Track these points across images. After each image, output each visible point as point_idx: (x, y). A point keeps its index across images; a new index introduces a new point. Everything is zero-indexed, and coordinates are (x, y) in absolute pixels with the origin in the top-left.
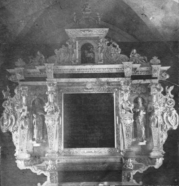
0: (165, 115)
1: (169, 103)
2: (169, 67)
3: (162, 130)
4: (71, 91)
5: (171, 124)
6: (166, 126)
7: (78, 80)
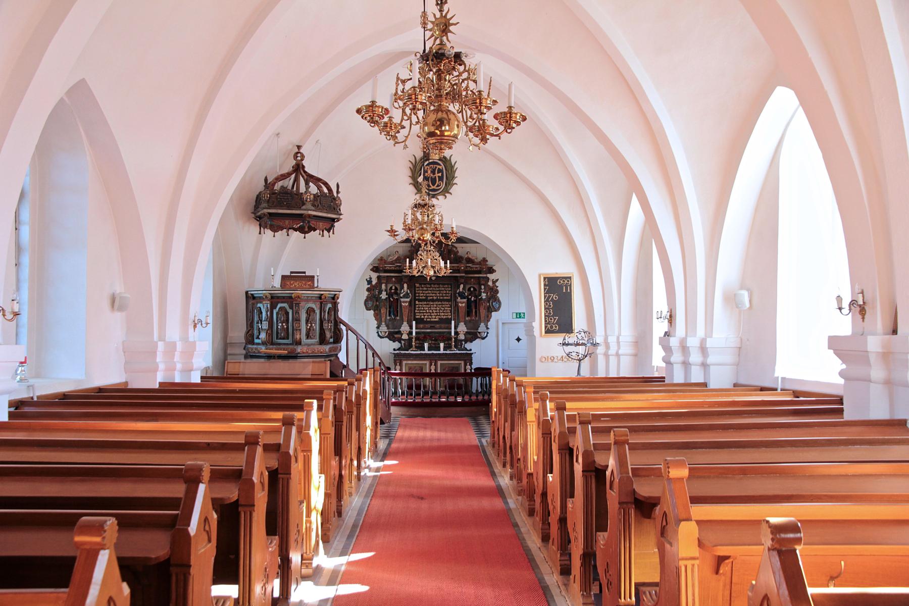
0: (491, 302)
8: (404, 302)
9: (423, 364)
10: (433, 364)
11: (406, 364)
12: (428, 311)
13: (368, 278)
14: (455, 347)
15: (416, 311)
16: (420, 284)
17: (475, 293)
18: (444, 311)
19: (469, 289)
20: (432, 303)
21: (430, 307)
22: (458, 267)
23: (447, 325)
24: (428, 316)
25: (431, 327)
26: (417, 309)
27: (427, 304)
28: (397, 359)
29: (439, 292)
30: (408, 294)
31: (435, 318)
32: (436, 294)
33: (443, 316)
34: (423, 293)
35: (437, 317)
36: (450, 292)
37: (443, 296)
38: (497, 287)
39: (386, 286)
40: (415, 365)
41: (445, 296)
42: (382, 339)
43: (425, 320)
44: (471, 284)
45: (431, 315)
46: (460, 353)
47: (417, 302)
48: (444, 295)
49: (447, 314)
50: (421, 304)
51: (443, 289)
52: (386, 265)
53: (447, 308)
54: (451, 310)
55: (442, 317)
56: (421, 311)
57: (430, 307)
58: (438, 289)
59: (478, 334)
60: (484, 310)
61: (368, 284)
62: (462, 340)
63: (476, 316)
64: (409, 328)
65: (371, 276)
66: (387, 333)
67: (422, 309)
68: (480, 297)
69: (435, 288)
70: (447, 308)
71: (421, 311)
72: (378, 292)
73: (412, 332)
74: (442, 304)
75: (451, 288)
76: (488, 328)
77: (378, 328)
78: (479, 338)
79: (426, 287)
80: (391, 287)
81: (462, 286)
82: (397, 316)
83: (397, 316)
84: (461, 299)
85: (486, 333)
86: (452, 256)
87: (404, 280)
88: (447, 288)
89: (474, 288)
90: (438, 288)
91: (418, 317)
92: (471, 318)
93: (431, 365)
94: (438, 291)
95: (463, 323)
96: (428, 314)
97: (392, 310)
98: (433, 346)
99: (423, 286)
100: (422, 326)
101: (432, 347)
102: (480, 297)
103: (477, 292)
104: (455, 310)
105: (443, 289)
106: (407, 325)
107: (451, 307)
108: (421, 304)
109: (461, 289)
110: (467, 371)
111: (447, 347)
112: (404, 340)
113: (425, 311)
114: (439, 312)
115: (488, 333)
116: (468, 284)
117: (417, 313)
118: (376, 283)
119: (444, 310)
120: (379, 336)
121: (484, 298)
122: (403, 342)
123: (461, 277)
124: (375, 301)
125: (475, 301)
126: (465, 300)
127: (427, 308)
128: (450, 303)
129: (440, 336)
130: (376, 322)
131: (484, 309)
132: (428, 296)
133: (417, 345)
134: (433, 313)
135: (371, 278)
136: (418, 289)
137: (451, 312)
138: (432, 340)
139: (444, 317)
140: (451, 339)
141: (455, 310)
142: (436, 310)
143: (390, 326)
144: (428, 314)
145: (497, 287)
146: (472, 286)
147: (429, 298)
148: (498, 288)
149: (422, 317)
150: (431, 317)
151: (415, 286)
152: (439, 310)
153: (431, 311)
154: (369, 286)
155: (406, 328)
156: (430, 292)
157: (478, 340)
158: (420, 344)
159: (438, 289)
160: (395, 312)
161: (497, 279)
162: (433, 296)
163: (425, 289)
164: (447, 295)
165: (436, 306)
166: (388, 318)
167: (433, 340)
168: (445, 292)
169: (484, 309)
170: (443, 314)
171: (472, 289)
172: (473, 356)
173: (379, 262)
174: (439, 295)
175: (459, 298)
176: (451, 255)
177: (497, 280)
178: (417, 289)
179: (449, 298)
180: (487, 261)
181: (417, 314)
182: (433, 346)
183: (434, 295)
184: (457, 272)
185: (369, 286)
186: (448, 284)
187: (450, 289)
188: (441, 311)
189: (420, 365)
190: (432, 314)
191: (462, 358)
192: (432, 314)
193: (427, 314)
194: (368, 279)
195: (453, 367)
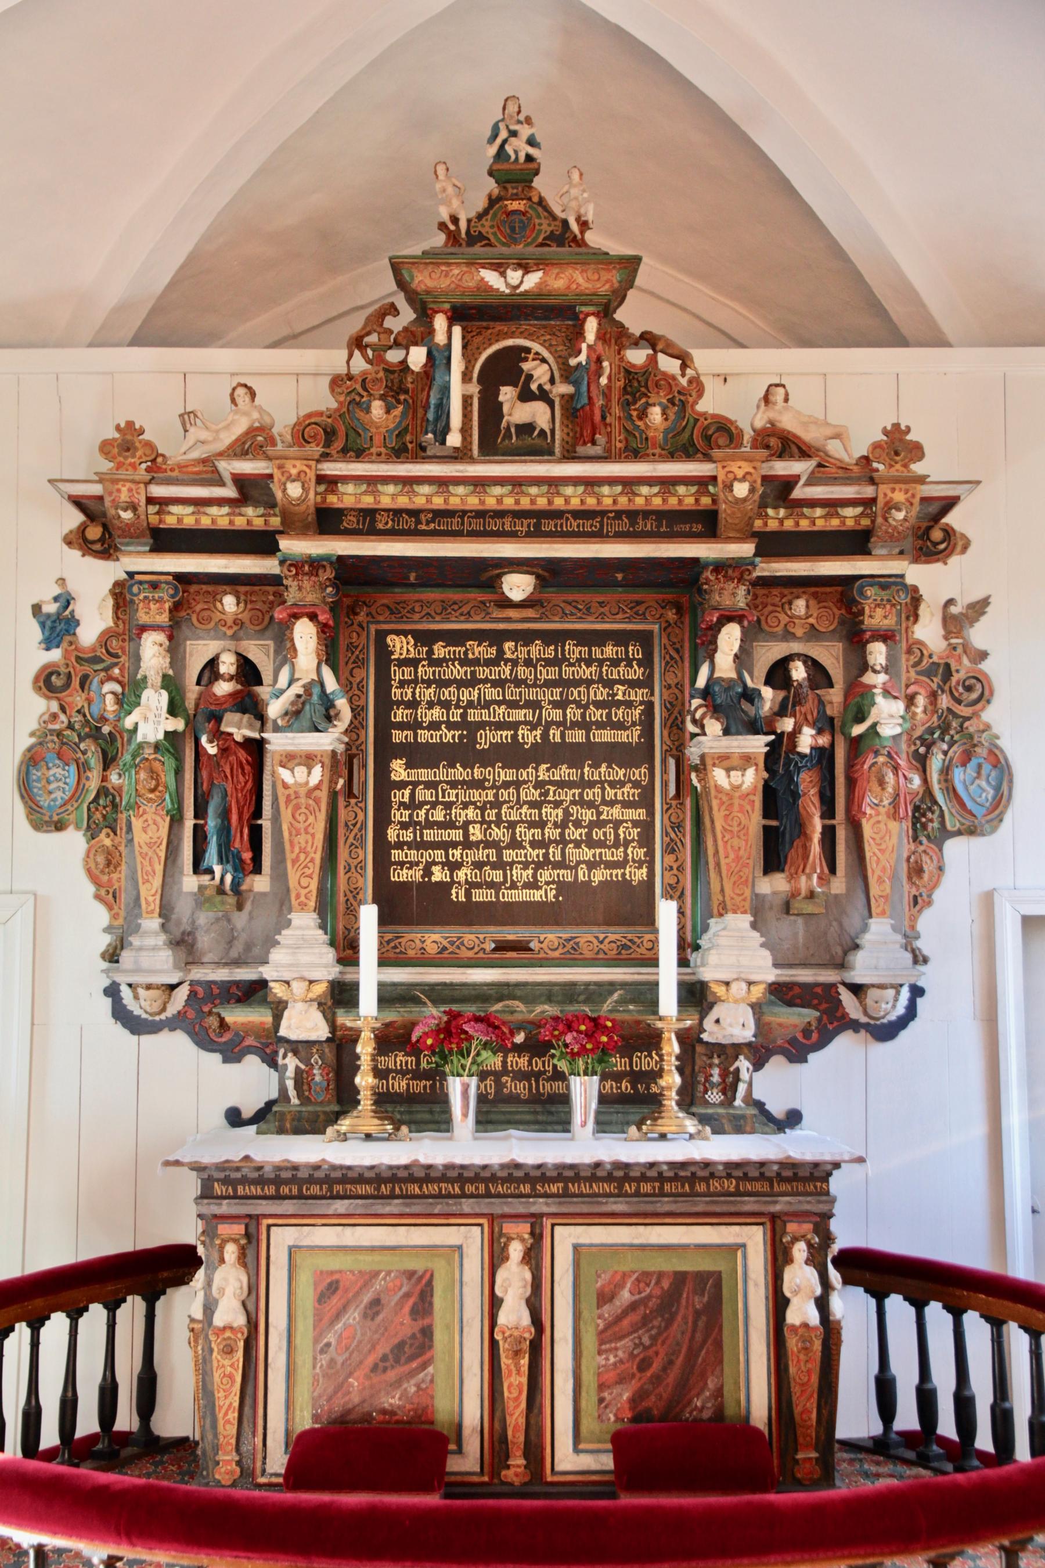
0: (936, 763)
1: (961, 689)
2: (941, 1451)
3: (915, 838)
4: (381, 618)
5: (969, 805)
6: (942, 815)
7: (597, 551)
8: (289, 759)
9: (431, 1249)
10: (516, 1250)
11: (292, 1251)
12: (476, 833)
13: (46, 594)
14: (688, 1099)
15: (392, 834)
16: (425, 638)
17: (821, 703)
18: (598, 834)
19: (778, 676)
20: (506, 775)
21: (497, 804)
22: (703, 483)
23: (615, 935)
24: (478, 865)
25: (502, 947)
26: (399, 815)
27: (479, 784)
28: (225, 1208)
29: (556, 693)
30: (328, 703)
31: (533, 885)
32: (534, 705)
33: (592, 865)
34: (446, 705)
35: (545, 875)
36: (639, 695)
37: (585, 725)
38: (983, 655)
39: (175, 650)
40: (366, 1263)
41: (601, 725)
42: (147, 1040)
43: (458, 895)
44: (788, 636)
45: (500, 865)
46: (735, 1169)
47: (399, 770)
48: (598, 715)
49: (619, 854)
50: (431, 785)
51: (587, 672)
52: (158, 491)
53: (616, 812)
54: (646, 828)
55: (582, 874)
56: (429, 835)
57: (497, 804)
58: (552, 673)
59: (846, 997)
60: (894, 826)
61: (49, 643)
62: (737, 1049)
63: (833, 870)
64: (330, 955)
65: (72, 587)
66: (182, 994)
67: (439, 815)
68: (857, 730)
69: (528, 663)
70: (616, 812)
71: (429, 835)
72: (119, 700)
73: (354, 987)
74: (584, 784)
75: (647, 662)
76: (919, 959)
77: (112, 956)
78: (855, 1026)
79: (464, 662)
80: (212, 664)
81: (730, 638)
82: (257, 869)
83: (257, 869)
84: (726, 732)
85: (905, 994)
86: (655, 414)
87: (292, 596)
88: (615, 663)
89: (815, 667)
90: (549, 663)
91: (404, 875)
92: (791, 878)
93: (496, 1258)
94: (549, 684)
95: (741, 921)
96: (481, 854)
97: (212, 823)
98: (520, 1088)
99: (440, 650)
100: (432, 938)
101: (513, 1099)
102: (857, 730)
103: (835, 696)
104: (678, 826)
105: (587, 672)
106: (322, 937)
107: (646, 801)
108: (431, 785)
109: (725, 663)
110: (434, 879)
111: (623, 1099)
112: (297, 1047)
113: (457, 835)
114: (563, 842)
115: (917, 992)
116: (773, 637)
117: (399, 845)
118: (106, 638)
119: (600, 824)
120: (121, 1014)
121: (889, 730)
122: (291, 1063)
123: (720, 567)
124: (95, 761)
125: (824, 757)
126: (758, 744)
127: (471, 813)
128: (639, 773)
129: (569, 1027)
130: (102, 916)
131: (894, 815)
132: (482, 725)
133: (399, 1085)
134: (515, 844)
135: (66, 600)
136: (407, 673)
137: (646, 840)
138: (502, 1047)
139: (599, 876)
140: (652, 1040)
141: (678, 826)
142: (541, 824)
143: (204, 941)
144: (481, 854)
145: (983, 655)
146: (796, 647)
147: (486, 739)
148: (985, 666)
149: (438, 875)
150: (497, 876)
151: (384, 654)
152: (563, 825)
153: (498, 833)
154: (55, 655)
155: (305, 957)
156: (492, 693)
157: (844, 1044)
158: (418, 1075)
159: (552, 673)
160: (240, 843)
161: (976, 596)
162: (514, 726)
163: (457, 671)
164: (619, 714)
165: (535, 794)
166: (190, 882)
167: (518, 1049)
168: (601, 693)
169: (894, 815)
170: (588, 854)
171: (799, 672)
172: (837, 1184)
173: (106, 466)
174: (556, 715)
175: (714, 727)
176: (643, 414)
177: (979, 607)
178: (398, 674)
179: (632, 736)
180: (917, 451)
181: (396, 855)
182: (520, 1088)
183: (519, 715)
184: (698, 528)
185: (55, 655)
186: (621, 638)
187: (636, 673)
188: (574, 833)
189: (418, 1265)
190: (509, 855)
191: (750, 1204)
192: (509, 855)
193: (471, 856)
194: (51, 608)
195: (680, 1278)
